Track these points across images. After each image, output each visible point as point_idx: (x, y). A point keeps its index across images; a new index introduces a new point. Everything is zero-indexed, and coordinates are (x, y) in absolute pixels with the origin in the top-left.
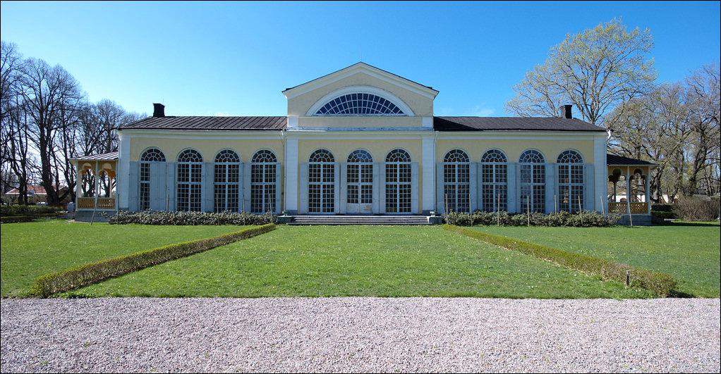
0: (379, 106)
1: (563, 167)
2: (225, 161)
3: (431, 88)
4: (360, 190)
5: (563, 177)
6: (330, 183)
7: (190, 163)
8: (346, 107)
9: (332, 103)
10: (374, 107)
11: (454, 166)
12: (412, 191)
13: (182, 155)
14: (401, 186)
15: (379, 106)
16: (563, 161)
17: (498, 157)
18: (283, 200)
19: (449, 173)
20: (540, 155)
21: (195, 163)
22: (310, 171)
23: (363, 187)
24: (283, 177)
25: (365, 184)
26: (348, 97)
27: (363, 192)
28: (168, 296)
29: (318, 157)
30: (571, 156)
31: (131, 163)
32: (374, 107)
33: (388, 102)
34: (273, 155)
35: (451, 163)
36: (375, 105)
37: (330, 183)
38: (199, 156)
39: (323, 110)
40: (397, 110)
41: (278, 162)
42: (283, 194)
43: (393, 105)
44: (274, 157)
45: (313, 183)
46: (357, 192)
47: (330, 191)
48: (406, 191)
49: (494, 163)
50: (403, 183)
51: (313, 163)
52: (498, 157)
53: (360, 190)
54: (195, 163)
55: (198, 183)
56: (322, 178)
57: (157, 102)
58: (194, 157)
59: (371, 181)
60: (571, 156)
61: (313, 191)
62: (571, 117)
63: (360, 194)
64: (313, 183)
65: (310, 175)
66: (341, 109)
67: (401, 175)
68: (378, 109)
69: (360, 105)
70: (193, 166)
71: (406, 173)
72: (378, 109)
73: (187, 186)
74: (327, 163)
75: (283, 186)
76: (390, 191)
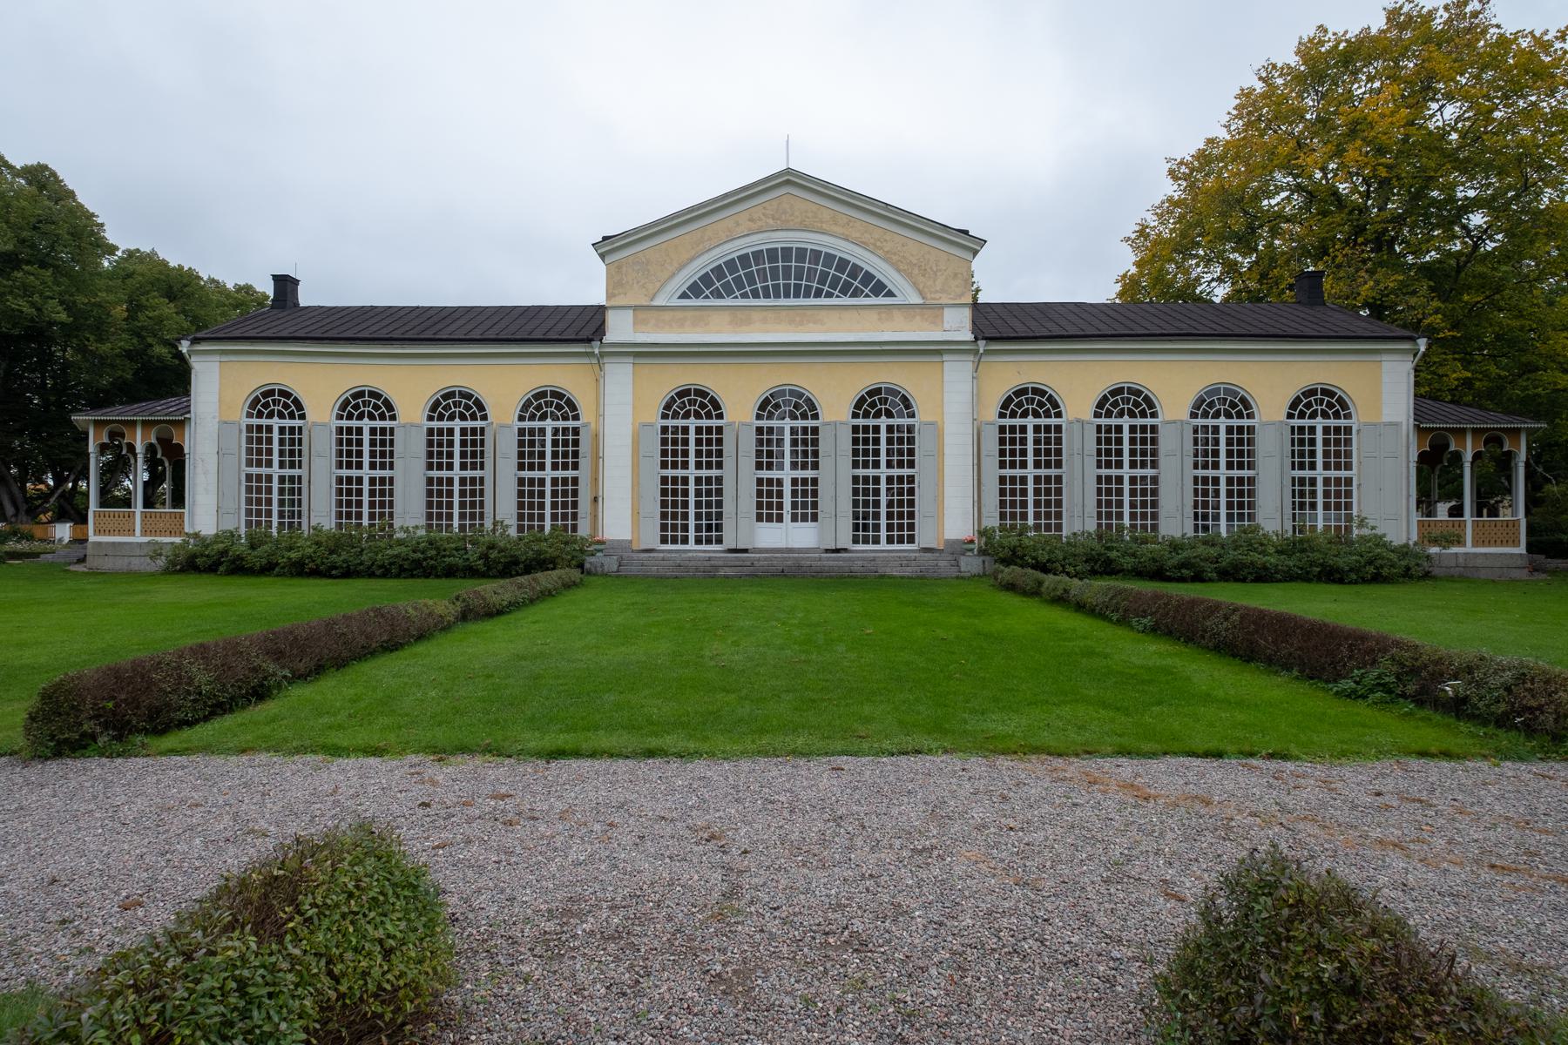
0: (836, 280)
1: (1301, 429)
2: (360, 417)
3: (966, 232)
4: (787, 489)
5: (1205, 453)
6: (714, 473)
7: (366, 424)
8: (752, 281)
9: (718, 271)
10: (822, 281)
11: (451, 431)
12: (515, 494)
13: (346, 403)
14: (698, 480)
15: (836, 280)
16: (1302, 415)
17: (1137, 404)
18: (595, 517)
19: (1010, 445)
20: (1147, 400)
21: (378, 424)
22: (430, 443)
23: (794, 482)
24: (597, 458)
25: (800, 474)
26: (758, 255)
27: (794, 493)
28: (906, 753)
29: (1019, 405)
30: (1322, 401)
31: (224, 423)
32: (822, 281)
33: (856, 269)
34: (297, 402)
35: (445, 424)
36: (824, 276)
37: (714, 473)
38: (480, 406)
39: (694, 290)
40: (879, 289)
41: (584, 419)
42: (596, 499)
43: (868, 277)
44: (573, 407)
45: (435, 474)
46: (780, 494)
47: (712, 491)
48: (905, 492)
49: (1126, 422)
50: (560, 474)
51: (1008, 422)
52: (1330, 405)
53: (787, 489)
54: (378, 424)
55: (386, 473)
56: (883, 458)
57: (281, 271)
58: (468, 408)
59: (815, 466)
60: (1322, 401)
61: (671, 492)
62: (600, 311)
63: (787, 500)
64: (435, 474)
65: (430, 455)
66: (740, 286)
67: (1326, 454)
68: (833, 286)
69: (787, 276)
70: (373, 431)
71: (904, 447)
72: (833, 286)
73: (360, 480)
74: (1139, 421)
75: (596, 480)
76: (863, 491)
